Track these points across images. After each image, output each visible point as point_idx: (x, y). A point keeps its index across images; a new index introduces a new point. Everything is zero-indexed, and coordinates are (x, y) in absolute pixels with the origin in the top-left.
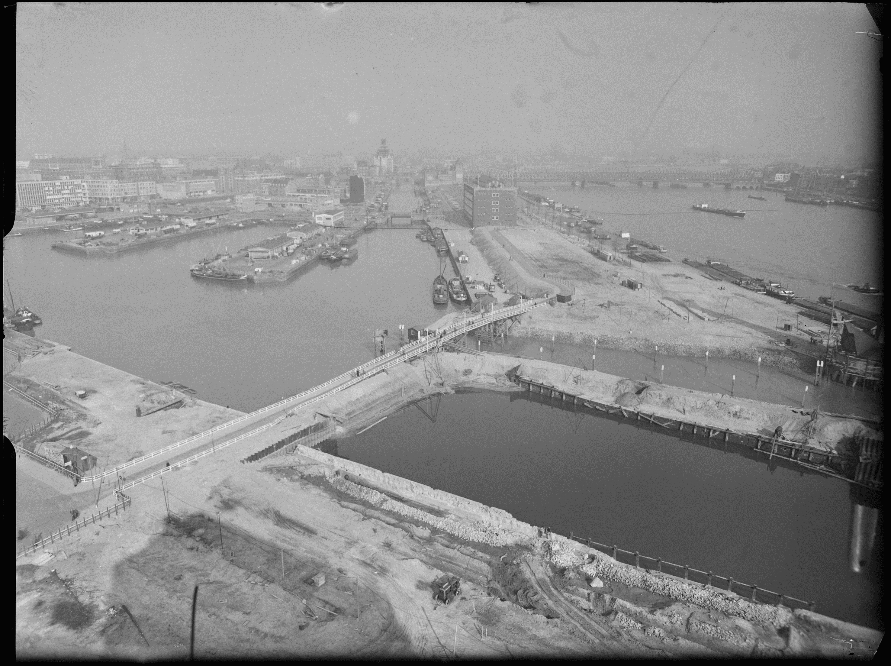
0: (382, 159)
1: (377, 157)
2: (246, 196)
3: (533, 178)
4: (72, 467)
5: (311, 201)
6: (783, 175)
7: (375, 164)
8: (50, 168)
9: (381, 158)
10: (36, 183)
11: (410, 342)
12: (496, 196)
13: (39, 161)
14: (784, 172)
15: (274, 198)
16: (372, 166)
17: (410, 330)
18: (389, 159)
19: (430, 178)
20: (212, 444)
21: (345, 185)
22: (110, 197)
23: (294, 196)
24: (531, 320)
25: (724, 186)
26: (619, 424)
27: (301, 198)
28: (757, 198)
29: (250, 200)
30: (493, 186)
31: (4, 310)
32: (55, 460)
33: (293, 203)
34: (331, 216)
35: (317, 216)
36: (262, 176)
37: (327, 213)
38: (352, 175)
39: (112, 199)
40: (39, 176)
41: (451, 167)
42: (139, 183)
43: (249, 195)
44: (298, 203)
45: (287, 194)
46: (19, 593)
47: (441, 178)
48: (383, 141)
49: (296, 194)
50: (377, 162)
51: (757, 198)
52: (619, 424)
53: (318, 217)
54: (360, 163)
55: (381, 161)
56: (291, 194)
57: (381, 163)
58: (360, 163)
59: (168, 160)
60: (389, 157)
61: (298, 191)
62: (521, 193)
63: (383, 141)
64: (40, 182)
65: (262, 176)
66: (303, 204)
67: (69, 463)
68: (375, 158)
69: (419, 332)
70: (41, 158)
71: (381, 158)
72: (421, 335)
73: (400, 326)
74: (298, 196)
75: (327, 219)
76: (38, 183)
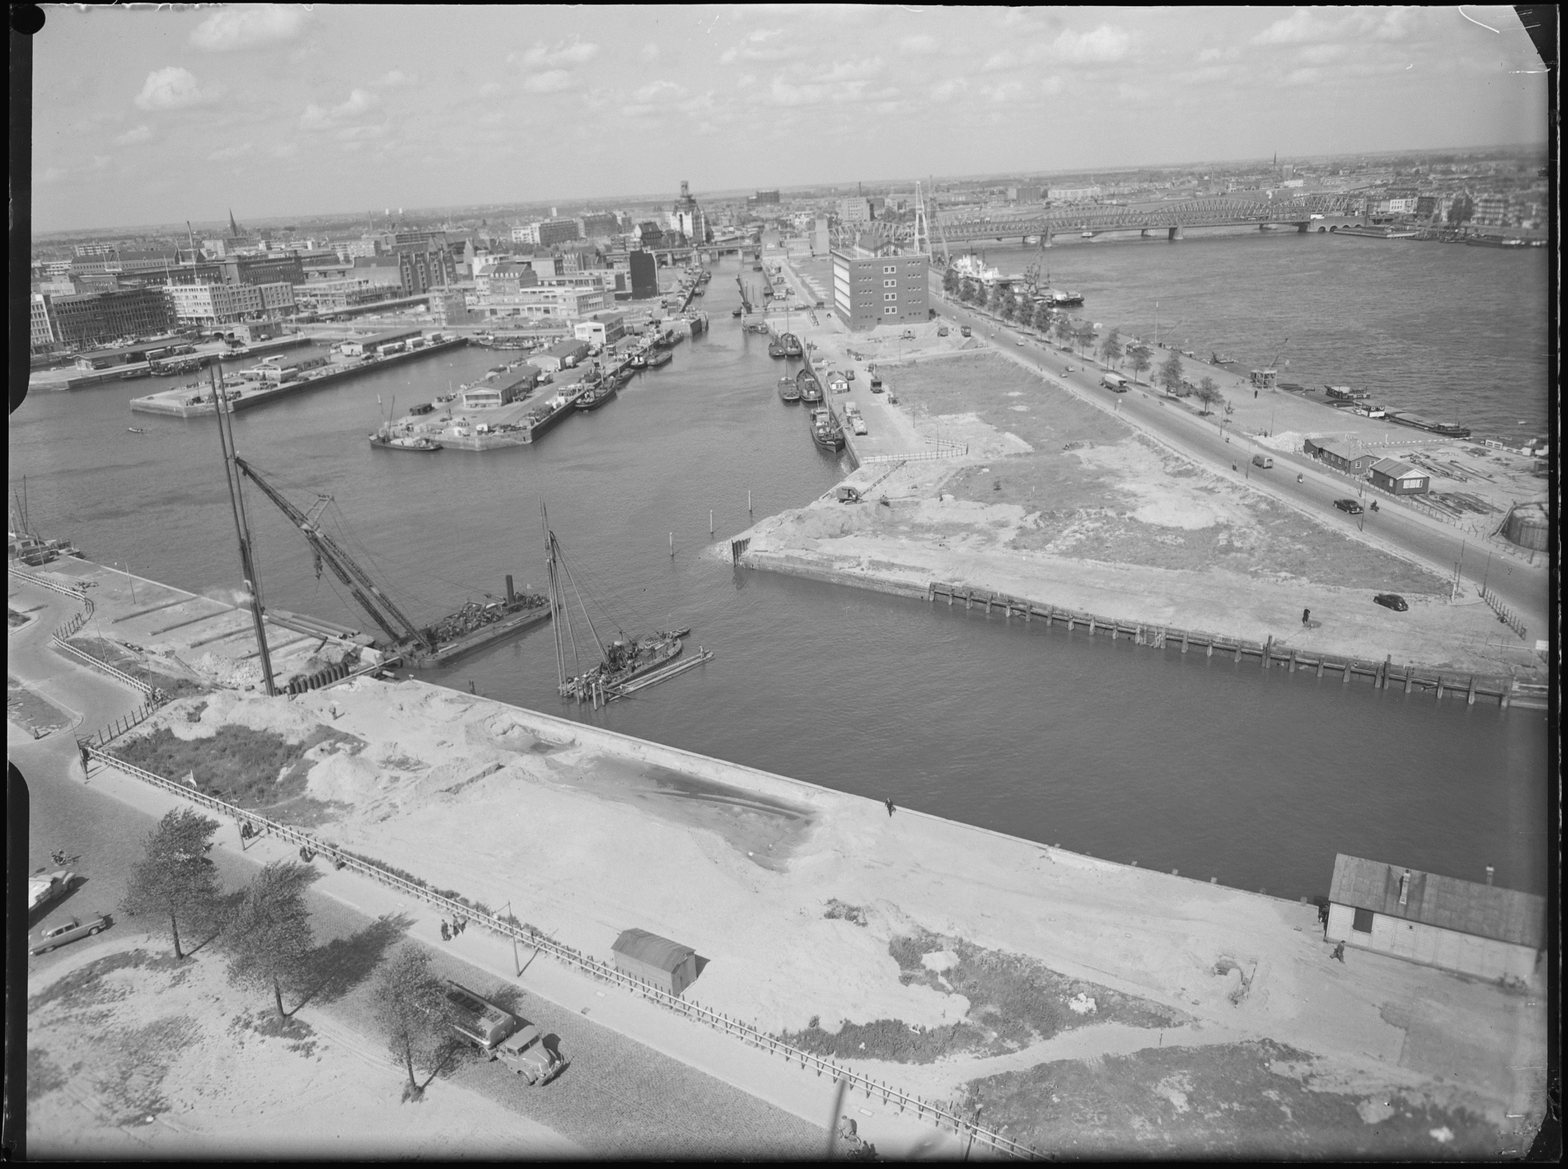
3: (953, 234)
5: (565, 300)
6: (1404, 201)
8: (107, 270)
9: (681, 216)
12: (889, 272)
14: (1405, 196)
15: (499, 298)
19: (771, 246)
21: (623, 268)
24: (424, 774)
25: (1297, 228)
26: (815, 1022)
27: (547, 297)
28: (253, 477)
30: (887, 254)
33: (534, 306)
38: (633, 250)
41: (808, 223)
44: (542, 306)
46: (32, 1011)
47: (791, 246)
48: (685, 186)
51: (253, 477)
52: (815, 1022)
53: (578, 329)
55: (681, 220)
66: (550, 306)
71: (681, 216)
74: (540, 292)
75: (595, 330)
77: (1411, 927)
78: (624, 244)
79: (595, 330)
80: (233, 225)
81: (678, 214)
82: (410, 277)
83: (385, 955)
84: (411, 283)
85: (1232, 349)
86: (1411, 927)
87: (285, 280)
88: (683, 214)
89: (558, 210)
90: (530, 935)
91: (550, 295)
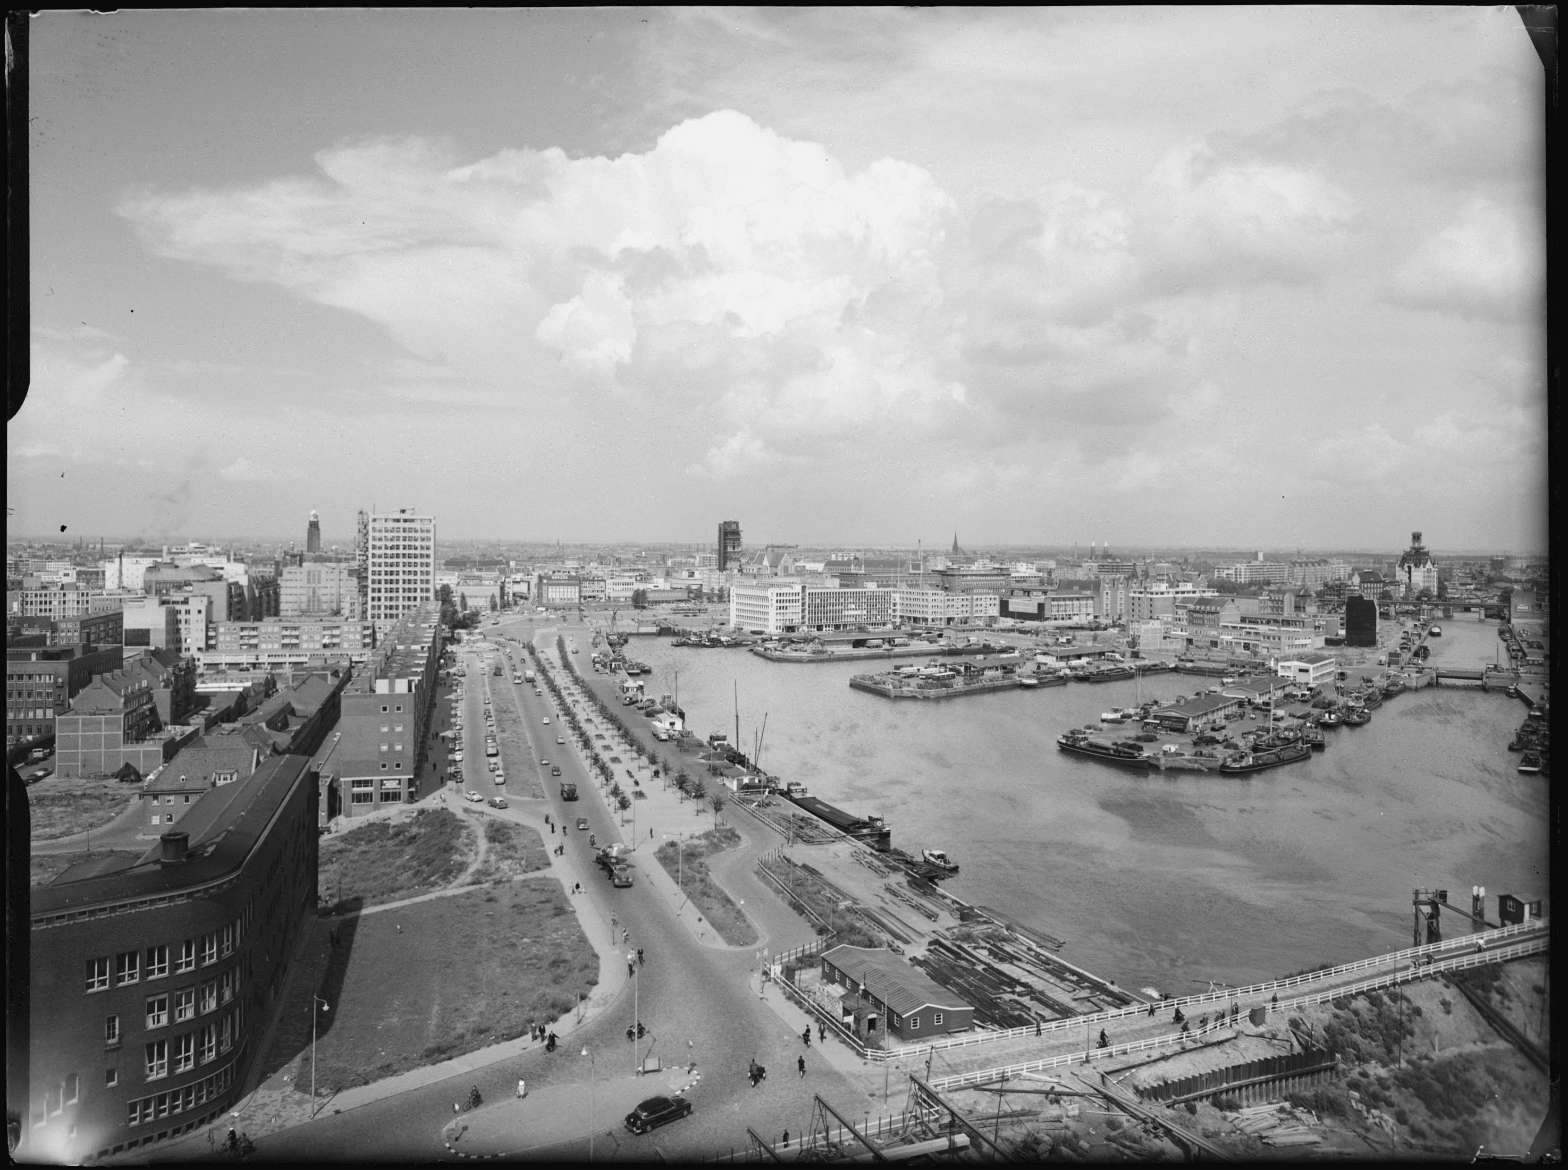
0: (1413, 569)
1: (1402, 566)
2: (1148, 623)
4: (853, 1026)
7: (1397, 578)
9: (1409, 568)
10: (832, 591)
11: (1503, 925)
13: (836, 563)
16: (1392, 583)
17: (1504, 899)
18: (1429, 571)
20: (1086, 1045)
22: (930, 617)
23: (1234, 627)
27: (1249, 633)
29: (1155, 630)
31: (36, 952)
32: (828, 1009)
34: (1310, 667)
35: (1280, 664)
36: (1177, 593)
37: (1300, 659)
39: (933, 620)
40: (837, 582)
42: (975, 597)
43: (1153, 621)
45: (1221, 624)
48: (1417, 537)
49: (1239, 625)
50: (1401, 575)
54: (1366, 578)
55: (1410, 572)
56: (1230, 625)
57: (1410, 578)
58: (1366, 578)
59: (1019, 565)
60: (1429, 565)
61: (1243, 620)
62: (350, 851)
63: (1417, 537)
64: (838, 590)
65: (1177, 593)
67: (850, 1019)
68: (1398, 569)
69: (1527, 908)
70: (840, 559)
71: (1409, 568)
72: (1531, 914)
73: (1475, 888)
75: (1301, 670)
76: (835, 591)
77: (700, 920)
78: (1339, 591)
79: (1301, 670)
80: (955, 547)
81: (1406, 565)
82: (1109, 602)
83: (191, 722)
84: (1109, 607)
85: (925, 646)
86: (700, 920)
87: (994, 594)
88: (1412, 565)
89: (1264, 555)
90: (931, 1084)
91: (1252, 631)
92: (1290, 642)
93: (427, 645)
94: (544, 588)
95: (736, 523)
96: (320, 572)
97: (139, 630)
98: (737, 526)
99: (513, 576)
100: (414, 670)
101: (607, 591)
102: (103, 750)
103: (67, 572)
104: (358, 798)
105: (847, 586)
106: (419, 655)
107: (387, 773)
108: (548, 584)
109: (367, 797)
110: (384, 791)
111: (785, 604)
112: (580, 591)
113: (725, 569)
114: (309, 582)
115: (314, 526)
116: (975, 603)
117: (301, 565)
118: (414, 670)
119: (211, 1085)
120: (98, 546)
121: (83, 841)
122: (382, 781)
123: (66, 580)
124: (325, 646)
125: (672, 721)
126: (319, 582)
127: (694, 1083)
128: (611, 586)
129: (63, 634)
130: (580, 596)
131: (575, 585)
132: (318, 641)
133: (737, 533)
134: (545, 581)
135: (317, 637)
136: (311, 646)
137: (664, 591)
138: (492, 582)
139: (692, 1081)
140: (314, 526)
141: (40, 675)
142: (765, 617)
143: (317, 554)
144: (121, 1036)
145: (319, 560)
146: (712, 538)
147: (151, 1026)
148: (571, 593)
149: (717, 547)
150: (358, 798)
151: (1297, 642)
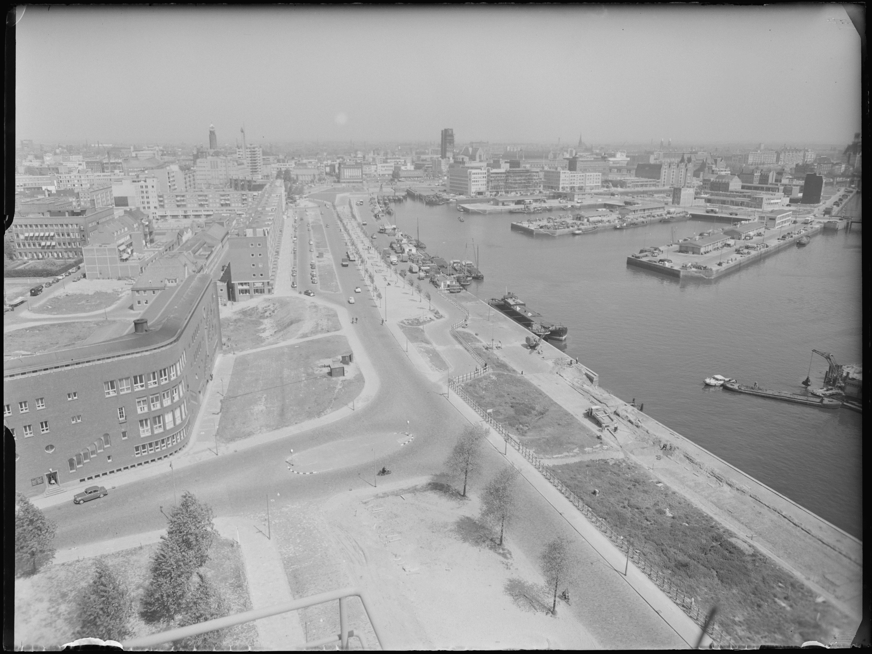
2: (686, 190)
9: (850, 155)
71: (850, 155)
80: (580, 142)
81: (848, 153)
88: (852, 153)
92: (768, 201)
93: (274, 208)
94: (342, 170)
95: (452, 130)
96: (217, 162)
97: (121, 197)
98: (452, 132)
99: (325, 162)
100: (267, 223)
101: (378, 171)
102: (109, 265)
103: (80, 163)
104: (242, 291)
105: (514, 167)
106: (270, 214)
107: (256, 279)
108: (344, 168)
109: (246, 291)
110: (255, 289)
111: (477, 180)
112: (362, 172)
113: (445, 157)
114: (211, 168)
115: (212, 133)
116: (587, 177)
117: (206, 158)
118: (267, 223)
119: (174, 438)
120: (97, 145)
121: (102, 314)
122: (254, 283)
123: (80, 168)
124: (222, 205)
125: (410, 249)
126: (217, 168)
127: (308, 473)
128: (381, 168)
129: (82, 199)
130: (362, 174)
131: (359, 168)
132: (218, 203)
133: (452, 135)
134: (342, 166)
135: (218, 201)
136: (215, 205)
137: (410, 170)
138: (313, 167)
139: (410, 439)
140: (212, 133)
141: (72, 225)
142: (465, 186)
143: (216, 150)
144: (126, 417)
145: (217, 154)
146: (438, 139)
147: (139, 411)
148: (357, 172)
149: (440, 143)
150: (242, 291)
151: (772, 201)
